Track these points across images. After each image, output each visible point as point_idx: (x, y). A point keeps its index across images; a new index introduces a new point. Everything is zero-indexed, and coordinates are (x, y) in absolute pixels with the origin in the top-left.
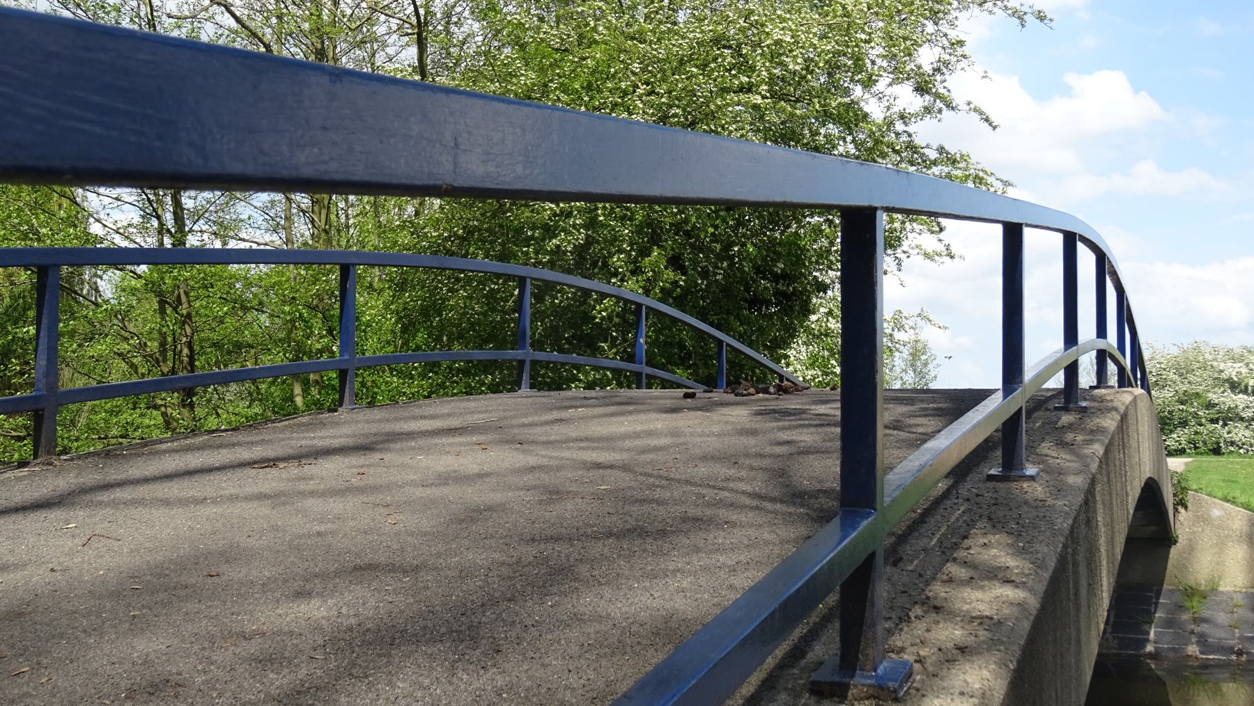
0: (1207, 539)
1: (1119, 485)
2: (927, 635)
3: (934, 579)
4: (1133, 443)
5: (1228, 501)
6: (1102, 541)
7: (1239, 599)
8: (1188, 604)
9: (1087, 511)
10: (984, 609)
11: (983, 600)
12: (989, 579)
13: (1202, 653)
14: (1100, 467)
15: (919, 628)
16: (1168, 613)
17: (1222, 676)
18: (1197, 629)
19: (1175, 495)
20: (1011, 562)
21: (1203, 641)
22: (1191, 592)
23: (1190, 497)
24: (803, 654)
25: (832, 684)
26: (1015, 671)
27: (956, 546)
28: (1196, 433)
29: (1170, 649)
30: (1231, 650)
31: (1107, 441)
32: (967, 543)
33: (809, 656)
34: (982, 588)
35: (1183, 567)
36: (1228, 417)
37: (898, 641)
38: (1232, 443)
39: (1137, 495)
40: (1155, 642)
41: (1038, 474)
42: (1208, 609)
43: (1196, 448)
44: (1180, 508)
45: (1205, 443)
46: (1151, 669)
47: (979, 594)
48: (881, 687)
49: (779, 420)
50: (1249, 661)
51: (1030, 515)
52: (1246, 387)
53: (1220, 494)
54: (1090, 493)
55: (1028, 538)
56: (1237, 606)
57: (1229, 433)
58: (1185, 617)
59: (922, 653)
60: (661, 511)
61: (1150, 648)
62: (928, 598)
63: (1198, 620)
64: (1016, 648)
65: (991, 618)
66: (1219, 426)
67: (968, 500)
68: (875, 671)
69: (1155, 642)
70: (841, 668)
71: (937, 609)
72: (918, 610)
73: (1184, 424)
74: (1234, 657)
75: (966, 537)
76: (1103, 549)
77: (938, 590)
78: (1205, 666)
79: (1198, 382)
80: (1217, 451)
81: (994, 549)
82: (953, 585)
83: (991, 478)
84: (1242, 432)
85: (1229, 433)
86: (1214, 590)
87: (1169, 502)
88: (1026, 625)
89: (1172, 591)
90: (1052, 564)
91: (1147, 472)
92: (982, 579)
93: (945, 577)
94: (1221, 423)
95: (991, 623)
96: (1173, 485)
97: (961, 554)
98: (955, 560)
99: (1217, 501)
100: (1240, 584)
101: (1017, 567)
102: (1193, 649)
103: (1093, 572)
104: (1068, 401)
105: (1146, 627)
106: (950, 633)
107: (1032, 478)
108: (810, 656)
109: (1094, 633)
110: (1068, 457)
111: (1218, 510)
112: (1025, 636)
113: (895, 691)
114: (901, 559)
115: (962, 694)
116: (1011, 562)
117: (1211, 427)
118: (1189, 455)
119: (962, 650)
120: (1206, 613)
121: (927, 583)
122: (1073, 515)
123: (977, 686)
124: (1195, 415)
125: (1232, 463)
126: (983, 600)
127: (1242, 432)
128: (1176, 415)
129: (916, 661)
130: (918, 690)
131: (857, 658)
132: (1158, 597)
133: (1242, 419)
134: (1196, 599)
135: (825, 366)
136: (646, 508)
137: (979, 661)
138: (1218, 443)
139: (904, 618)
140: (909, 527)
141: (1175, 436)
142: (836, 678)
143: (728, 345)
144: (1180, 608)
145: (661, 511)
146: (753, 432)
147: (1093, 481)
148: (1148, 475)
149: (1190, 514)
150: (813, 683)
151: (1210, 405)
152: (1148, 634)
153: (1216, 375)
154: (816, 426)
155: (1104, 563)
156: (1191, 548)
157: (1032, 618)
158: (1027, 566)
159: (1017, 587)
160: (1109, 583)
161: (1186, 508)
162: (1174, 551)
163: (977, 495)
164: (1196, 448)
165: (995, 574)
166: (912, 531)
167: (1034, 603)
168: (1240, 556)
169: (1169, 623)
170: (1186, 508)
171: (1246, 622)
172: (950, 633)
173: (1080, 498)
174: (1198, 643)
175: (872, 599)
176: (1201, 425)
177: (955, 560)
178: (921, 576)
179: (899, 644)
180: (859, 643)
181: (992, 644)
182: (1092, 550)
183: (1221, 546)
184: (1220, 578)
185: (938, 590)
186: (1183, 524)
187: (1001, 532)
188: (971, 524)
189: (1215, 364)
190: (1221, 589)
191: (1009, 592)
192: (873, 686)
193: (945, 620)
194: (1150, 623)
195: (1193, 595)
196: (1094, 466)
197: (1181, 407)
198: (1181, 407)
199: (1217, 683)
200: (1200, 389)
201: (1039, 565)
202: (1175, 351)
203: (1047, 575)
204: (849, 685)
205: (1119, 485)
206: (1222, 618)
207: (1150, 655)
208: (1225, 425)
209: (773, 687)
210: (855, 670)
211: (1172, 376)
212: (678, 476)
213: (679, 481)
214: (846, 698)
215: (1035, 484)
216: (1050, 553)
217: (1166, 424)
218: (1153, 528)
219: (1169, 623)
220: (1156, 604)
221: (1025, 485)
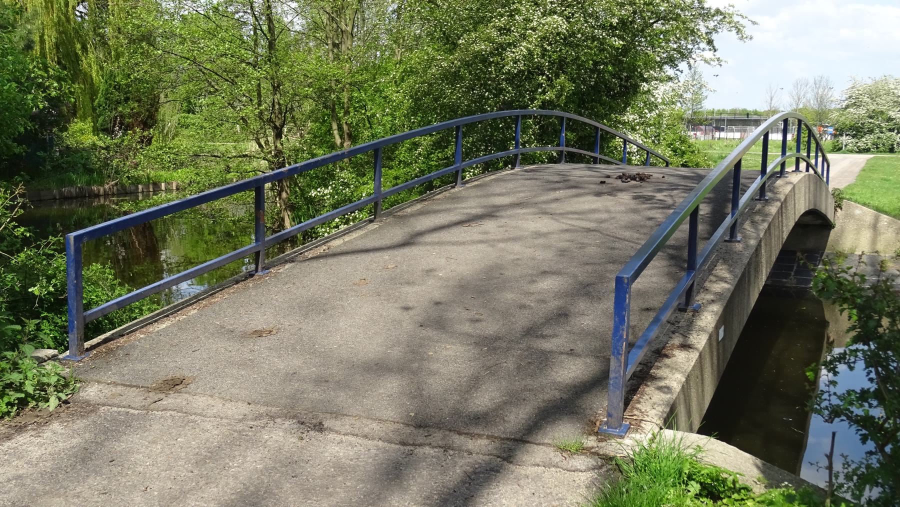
0: (851, 226)
10: (719, 290)
22: (840, 255)
27: (713, 269)
28: (879, 138)
35: (837, 241)
37: (697, 298)
39: (791, 228)
43: (877, 148)
45: (884, 145)
49: (644, 203)
73: (871, 131)
79: (883, 104)
80: (892, 150)
81: (722, 270)
88: (729, 294)
104: (761, 196)
106: (710, 297)
111: (859, 211)
118: (873, 153)
119: (713, 301)
124: (879, 126)
128: (866, 125)
135: (641, 113)
138: (892, 145)
139: (698, 292)
141: (864, 139)
143: (602, 130)
146: (635, 211)
147: (760, 241)
149: (843, 212)
151: (890, 119)
153: (896, 99)
154: (659, 208)
156: (842, 231)
164: (877, 148)
165: (722, 279)
181: (720, 300)
183: (858, 231)
185: (707, 284)
189: (896, 91)
191: (726, 286)
196: (762, 235)
200: (884, 108)
201: (735, 276)
202: (869, 82)
211: (866, 99)
216: (739, 272)
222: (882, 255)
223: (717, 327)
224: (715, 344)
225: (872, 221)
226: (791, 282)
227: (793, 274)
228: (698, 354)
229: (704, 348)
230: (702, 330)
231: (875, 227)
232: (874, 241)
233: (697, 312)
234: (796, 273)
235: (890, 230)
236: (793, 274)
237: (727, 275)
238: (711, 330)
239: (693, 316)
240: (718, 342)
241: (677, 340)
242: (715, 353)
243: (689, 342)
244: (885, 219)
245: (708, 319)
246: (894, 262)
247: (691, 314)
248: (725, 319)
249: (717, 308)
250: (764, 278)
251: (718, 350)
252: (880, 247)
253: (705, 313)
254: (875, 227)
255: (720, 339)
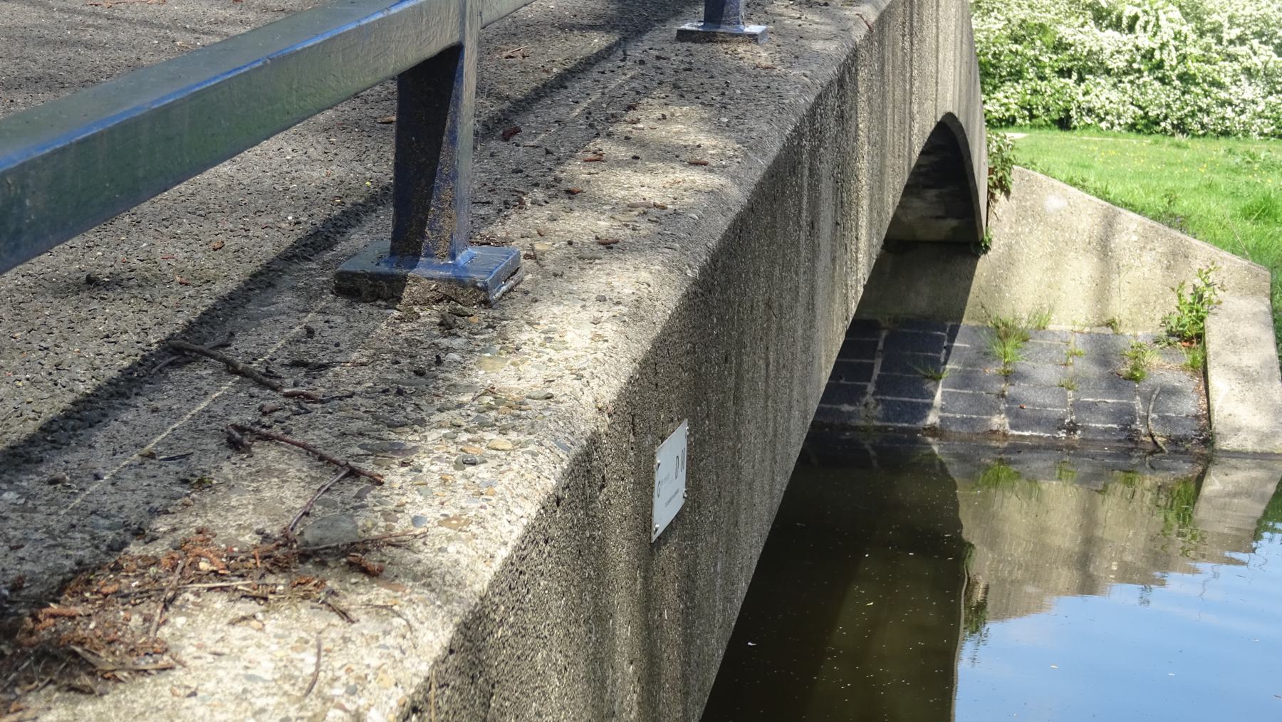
1: (898, 92)
2: (550, 225)
3: (571, 156)
4: (929, 32)
5: (1075, 185)
6: (863, 165)
7: (1078, 344)
8: (998, 350)
9: (841, 97)
10: (655, 197)
11: (652, 185)
12: (663, 160)
13: (1013, 427)
14: (869, 37)
15: (537, 216)
16: (965, 365)
17: (1040, 465)
18: (1010, 390)
19: (991, 171)
20: (705, 140)
21: (1018, 418)
22: (1003, 332)
23: (1015, 178)
24: (329, 244)
25: (375, 277)
26: (695, 282)
27: (613, 118)
28: (1035, 92)
29: (963, 421)
30: (1059, 424)
31: (884, 6)
32: (632, 114)
33: (339, 248)
34: (652, 171)
35: (995, 289)
36: (1084, 68)
38: (1090, 111)
40: (942, 409)
41: (764, 33)
42: (1029, 358)
43: (1032, 117)
44: (997, 192)
45: (1047, 109)
46: (933, 454)
47: (647, 179)
48: (460, 282)
50: (1084, 440)
51: (743, 86)
52: (1119, 19)
53: (1064, 177)
54: (844, 80)
55: (737, 113)
56: (1073, 354)
57: (1086, 93)
58: (992, 370)
59: (538, 247)
60: (96, 57)
61: (932, 418)
62: (558, 180)
63: (1009, 376)
64: (700, 249)
65: (663, 208)
66: (1071, 82)
67: (642, 62)
68: (453, 257)
69: (942, 409)
70: (393, 252)
71: (571, 193)
72: (539, 194)
73: (1017, 75)
74: (1062, 434)
75: (630, 108)
76: (865, 192)
77: (576, 171)
78: (1017, 447)
80: (1064, 123)
82: (603, 165)
83: (683, 36)
84: (1106, 94)
85: (1086, 93)
86: (1040, 328)
87: (982, 182)
88: (722, 224)
89: (975, 330)
90: (774, 149)
91: (949, 102)
92: (652, 158)
93: (590, 156)
94: (1075, 76)
95: (662, 217)
96: (990, 155)
97: (622, 128)
98: (609, 135)
99: (1057, 183)
100: (1082, 320)
101: (715, 147)
102: (999, 421)
103: (843, 224)
105: (930, 385)
106: (586, 224)
107: (754, 38)
108: (342, 247)
109: (838, 309)
110: (817, 19)
112: (718, 237)
113: (485, 289)
114: (516, 131)
115: (602, 299)
116: (705, 140)
117: (1059, 82)
119: (608, 245)
120: (1024, 365)
121: (559, 162)
122: (817, 92)
123: (628, 291)
124: (1036, 62)
125: (1087, 143)
126: (652, 185)
127: (1106, 94)
128: (1006, 60)
129: (527, 257)
130: (526, 293)
131: (423, 235)
132: (952, 338)
133: (1108, 72)
134: (1012, 342)
136: (64, 54)
137: (631, 260)
138: (1067, 110)
140: (536, 90)
141: (1000, 95)
142: (384, 269)
144: (986, 355)
145: (96, 57)
147: (855, 54)
148: (950, 109)
149: (1013, 203)
150: (341, 276)
151: (1060, 47)
152: (933, 396)
155: (865, 203)
156: (1010, 261)
157: (731, 215)
158: (731, 146)
159: (711, 171)
160: (870, 245)
161: (1007, 193)
162: (984, 265)
163: (658, 58)
164: (1032, 117)
166: (540, 98)
167: (737, 195)
168: (1085, 274)
169: (966, 379)
170: (1007, 193)
171: (1086, 380)
172: (586, 224)
173: (831, 72)
174: (1008, 412)
175: (453, 132)
176: (1042, 78)
177: (609, 135)
178: (548, 152)
179: (501, 234)
180: (427, 209)
181: (654, 244)
182: (844, 177)
183: (1057, 257)
184: (1052, 309)
186: (1000, 220)
187: (692, 103)
188: (645, 92)
190: (1051, 327)
191: (697, 178)
192: (449, 280)
193: (584, 209)
194: (936, 379)
195: (1007, 335)
196: (859, 34)
197: (1014, 47)
198: (1014, 47)
199: (1033, 480)
200: (1046, 18)
203: (762, 164)
204: (405, 277)
205: (898, 92)
206: (1047, 373)
207: (933, 431)
208: (1081, 80)
209: (270, 285)
210: (419, 255)
212: (128, 15)
213: (130, 22)
214: (399, 300)
215: (757, 48)
217: (987, 74)
218: (953, 223)
219: (966, 379)
220: (949, 349)
221: (741, 49)
222: (1128, 332)
223: (638, 413)
224: (621, 552)
225: (1097, 231)
226: (867, 411)
227: (871, 388)
228: (434, 635)
229: (516, 568)
230: (509, 413)
231: (1104, 248)
232: (1102, 291)
233: (479, 304)
234: (881, 387)
235: (1148, 257)
236: (871, 388)
237: (709, 142)
238: (589, 421)
239: (446, 327)
240: (649, 548)
241: (263, 500)
242: (624, 631)
243: (370, 522)
244: (1131, 223)
245: (578, 345)
246: (1163, 353)
247: (429, 316)
248: (698, 362)
249: (648, 286)
250: (863, 272)
251: (648, 602)
252: (1120, 308)
253: (547, 312)
254: (1104, 248)
255: (662, 516)
